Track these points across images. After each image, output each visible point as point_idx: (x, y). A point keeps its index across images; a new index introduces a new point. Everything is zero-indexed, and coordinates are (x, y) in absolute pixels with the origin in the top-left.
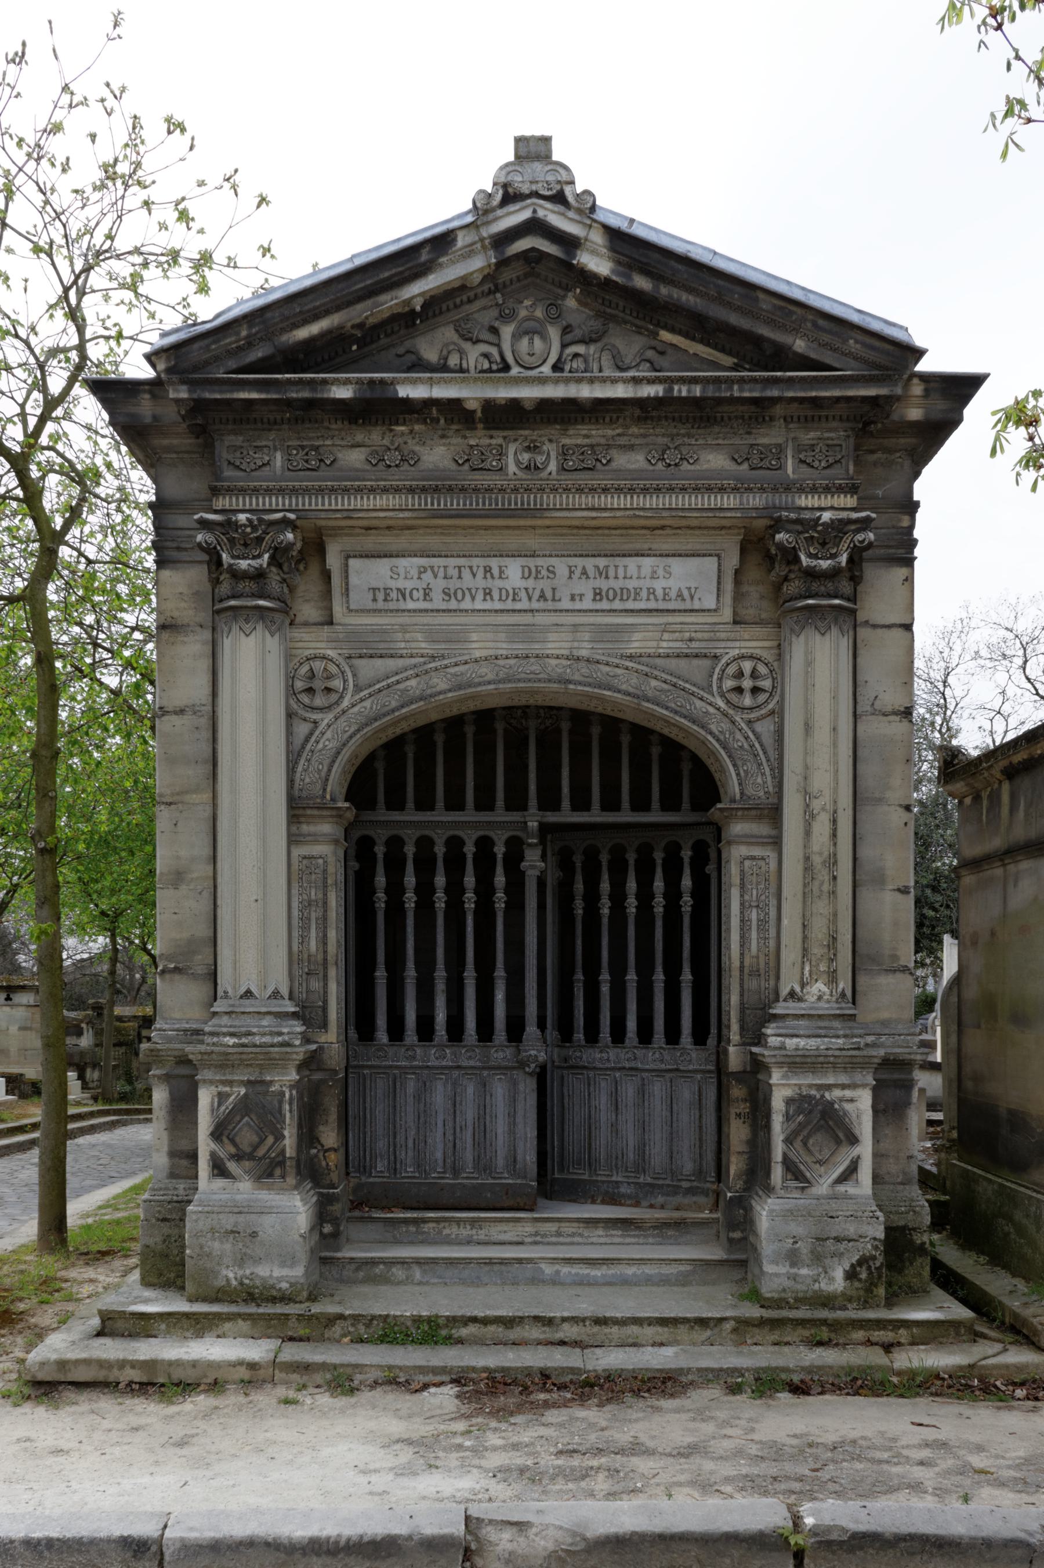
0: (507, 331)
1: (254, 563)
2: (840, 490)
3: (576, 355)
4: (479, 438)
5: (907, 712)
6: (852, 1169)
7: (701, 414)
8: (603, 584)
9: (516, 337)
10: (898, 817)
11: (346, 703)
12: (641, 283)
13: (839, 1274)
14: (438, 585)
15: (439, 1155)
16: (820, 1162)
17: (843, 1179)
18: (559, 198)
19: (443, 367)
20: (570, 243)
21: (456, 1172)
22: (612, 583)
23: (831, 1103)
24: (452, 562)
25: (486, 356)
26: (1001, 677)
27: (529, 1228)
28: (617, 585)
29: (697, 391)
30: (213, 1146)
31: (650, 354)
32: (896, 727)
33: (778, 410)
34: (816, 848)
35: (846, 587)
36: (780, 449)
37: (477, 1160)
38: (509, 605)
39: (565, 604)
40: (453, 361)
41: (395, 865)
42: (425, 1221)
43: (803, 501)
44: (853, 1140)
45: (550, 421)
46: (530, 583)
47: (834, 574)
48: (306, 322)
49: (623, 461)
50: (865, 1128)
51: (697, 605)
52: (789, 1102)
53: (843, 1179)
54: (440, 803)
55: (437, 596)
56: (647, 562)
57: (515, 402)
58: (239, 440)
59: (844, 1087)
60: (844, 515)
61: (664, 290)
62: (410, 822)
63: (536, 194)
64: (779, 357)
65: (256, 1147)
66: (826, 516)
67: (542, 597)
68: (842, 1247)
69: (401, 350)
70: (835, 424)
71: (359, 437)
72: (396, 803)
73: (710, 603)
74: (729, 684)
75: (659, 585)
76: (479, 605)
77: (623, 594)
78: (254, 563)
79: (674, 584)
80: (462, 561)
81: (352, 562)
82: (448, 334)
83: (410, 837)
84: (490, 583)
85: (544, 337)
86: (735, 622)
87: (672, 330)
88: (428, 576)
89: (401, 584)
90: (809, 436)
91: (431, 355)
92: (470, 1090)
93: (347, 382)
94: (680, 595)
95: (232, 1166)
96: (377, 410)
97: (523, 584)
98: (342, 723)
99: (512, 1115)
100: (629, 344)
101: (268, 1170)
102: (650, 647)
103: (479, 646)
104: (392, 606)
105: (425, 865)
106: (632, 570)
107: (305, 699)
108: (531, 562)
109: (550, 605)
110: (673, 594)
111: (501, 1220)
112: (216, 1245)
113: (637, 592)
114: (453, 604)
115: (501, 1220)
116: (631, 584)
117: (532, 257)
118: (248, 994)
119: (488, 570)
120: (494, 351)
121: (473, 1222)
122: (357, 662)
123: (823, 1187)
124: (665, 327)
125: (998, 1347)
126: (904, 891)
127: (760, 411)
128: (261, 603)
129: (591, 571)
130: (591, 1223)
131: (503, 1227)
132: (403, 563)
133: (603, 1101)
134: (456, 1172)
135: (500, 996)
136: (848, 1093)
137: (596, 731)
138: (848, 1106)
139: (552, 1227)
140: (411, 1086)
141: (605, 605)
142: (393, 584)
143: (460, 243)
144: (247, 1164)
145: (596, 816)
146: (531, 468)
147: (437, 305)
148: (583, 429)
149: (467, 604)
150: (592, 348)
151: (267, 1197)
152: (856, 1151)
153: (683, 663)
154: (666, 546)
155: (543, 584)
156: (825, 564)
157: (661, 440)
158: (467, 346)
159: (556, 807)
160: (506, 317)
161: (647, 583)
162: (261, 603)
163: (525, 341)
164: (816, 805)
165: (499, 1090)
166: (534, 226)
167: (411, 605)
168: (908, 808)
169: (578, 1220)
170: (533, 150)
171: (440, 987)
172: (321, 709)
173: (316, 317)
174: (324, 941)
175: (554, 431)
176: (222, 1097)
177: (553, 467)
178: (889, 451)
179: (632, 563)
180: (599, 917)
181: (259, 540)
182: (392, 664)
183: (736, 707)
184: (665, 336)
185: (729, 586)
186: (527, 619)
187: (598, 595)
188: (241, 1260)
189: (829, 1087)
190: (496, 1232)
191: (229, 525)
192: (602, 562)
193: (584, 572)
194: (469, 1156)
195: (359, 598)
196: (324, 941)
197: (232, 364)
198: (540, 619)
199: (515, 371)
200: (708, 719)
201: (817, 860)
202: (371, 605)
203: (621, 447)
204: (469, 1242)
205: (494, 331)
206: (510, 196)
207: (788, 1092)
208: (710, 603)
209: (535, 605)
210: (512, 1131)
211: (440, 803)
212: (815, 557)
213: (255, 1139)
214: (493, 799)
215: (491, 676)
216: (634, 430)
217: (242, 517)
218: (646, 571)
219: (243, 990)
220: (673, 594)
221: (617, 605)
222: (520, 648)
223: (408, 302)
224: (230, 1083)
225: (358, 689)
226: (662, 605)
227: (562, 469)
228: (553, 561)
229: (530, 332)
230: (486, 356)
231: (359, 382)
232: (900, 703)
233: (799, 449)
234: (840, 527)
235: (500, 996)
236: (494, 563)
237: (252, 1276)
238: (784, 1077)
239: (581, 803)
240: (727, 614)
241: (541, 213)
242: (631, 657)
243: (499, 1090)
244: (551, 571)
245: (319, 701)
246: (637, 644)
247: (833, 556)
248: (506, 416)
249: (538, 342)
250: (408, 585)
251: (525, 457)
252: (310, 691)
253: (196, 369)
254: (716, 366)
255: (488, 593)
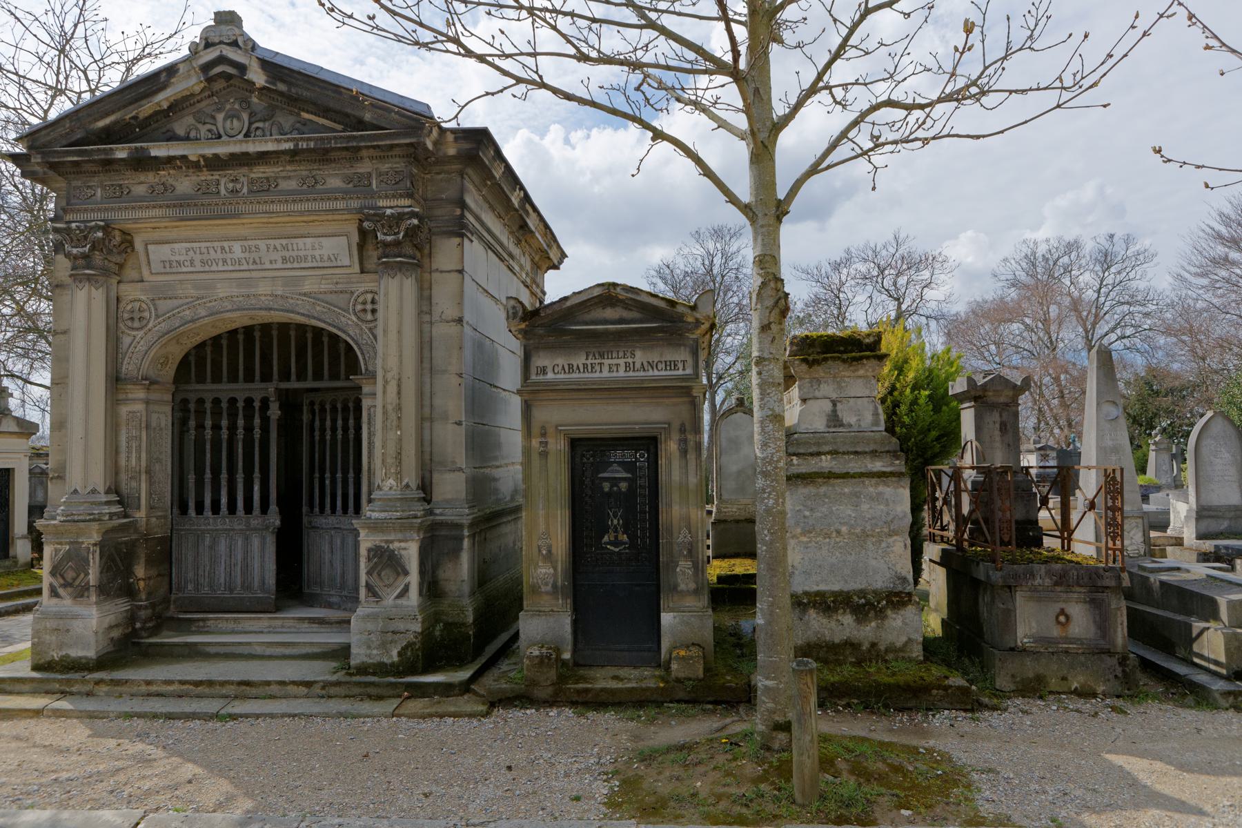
0: (220, 117)
1: (81, 250)
2: (401, 196)
3: (257, 128)
4: (205, 176)
5: (460, 321)
6: (406, 589)
7: (323, 155)
8: (287, 254)
9: (225, 119)
10: (455, 380)
11: (150, 325)
12: (282, 87)
13: (395, 653)
14: (198, 258)
15: (222, 580)
16: (388, 586)
17: (400, 596)
18: (235, 44)
19: (187, 138)
20: (242, 68)
21: (231, 591)
22: (291, 253)
23: (393, 551)
24: (203, 245)
25: (209, 131)
26: (869, 288)
27: (266, 623)
28: (294, 254)
29: (312, 145)
30: (51, 579)
31: (298, 125)
32: (453, 329)
33: (364, 153)
34: (389, 400)
35: (408, 250)
36: (370, 174)
37: (243, 583)
38: (237, 267)
39: (268, 266)
40: (193, 134)
41: (200, 413)
42: (208, 619)
43: (381, 203)
44: (406, 573)
45: (242, 165)
46: (247, 255)
47: (397, 243)
48: (102, 118)
49: (284, 185)
50: (413, 566)
51: (339, 264)
52: (369, 550)
53: (400, 596)
54: (209, 380)
55: (197, 263)
56: (309, 241)
57: (216, 156)
58: (79, 183)
59: (400, 541)
60: (400, 210)
61: (293, 90)
62: (209, 390)
63: (221, 43)
64: (361, 124)
65: (74, 580)
66: (389, 212)
67: (254, 262)
68: (396, 637)
69: (164, 130)
70: (398, 159)
71: (142, 178)
72: (201, 379)
73: (346, 262)
74: (359, 307)
75: (317, 253)
76: (221, 268)
77: (299, 259)
78: (81, 250)
79: (326, 252)
80: (208, 244)
81: (149, 247)
82: (190, 120)
83: (209, 398)
84: (225, 256)
85: (239, 119)
86: (362, 272)
87: (307, 112)
88: (191, 253)
89: (177, 258)
90: (385, 167)
91: (181, 131)
92: (240, 543)
93: (123, 149)
94: (329, 258)
95: (61, 591)
96: (141, 163)
97: (243, 255)
98: (149, 336)
99: (262, 557)
100: (287, 121)
101: (80, 593)
102: (315, 288)
103: (222, 291)
104: (174, 270)
105: (217, 413)
106: (301, 246)
107: (129, 323)
108: (245, 243)
109: (259, 267)
110: (325, 258)
111: (250, 619)
112: (48, 637)
113: (306, 257)
114: (207, 268)
115: (250, 619)
116: (302, 253)
117: (223, 75)
118: (76, 491)
119: (223, 248)
120: (214, 128)
121: (235, 619)
122: (157, 302)
123: (389, 600)
124: (303, 110)
125: (396, 702)
126: (459, 423)
127: (353, 153)
128: (87, 272)
129: (279, 247)
130: (312, 620)
131: (252, 623)
132: (176, 246)
133: (326, 548)
134: (231, 591)
135: (256, 488)
136: (403, 545)
137: (309, 336)
138: (403, 552)
139: (279, 623)
140: (208, 541)
141: (289, 265)
142: (173, 258)
143: (181, 71)
144: (70, 589)
145: (310, 384)
146: (234, 192)
147: (176, 107)
148: (262, 169)
149: (214, 268)
150: (267, 124)
151: (78, 609)
152: (408, 579)
153: (334, 296)
154: (320, 230)
155: (254, 255)
156: (389, 238)
157: (304, 173)
158: (200, 126)
159: (288, 379)
160: (219, 110)
161: (310, 253)
162: (87, 272)
163: (229, 122)
164: (389, 376)
165: (256, 542)
166: (222, 60)
167: (184, 269)
168: (460, 375)
169: (293, 618)
170: (228, 19)
171: (224, 483)
172: (137, 329)
173: (107, 115)
174: (139, 459)
175: (244, 170)
176: (57, 551)
177: (245, 190)
178: (449, 173)
179: (300, 241)
180: (253, 441)
181: (86, 237)
182: (176, 302)
183: (363, 321)
184: (305, 115)
185: (355, 253)
186: (247, 275)
187: (284, 260)
188: (61, 646)
189: (392, 542)
190: (248, 625)
191: (68, 231)
192: (284, 242)
193: (275, 248)
194: (239, 581)
195: (156, 267)
196: (139, 459)
197: (64, 142)
198: (254, 274)
199: (224, 138)
200: (348, 327)
201: (390, 408)
202: (163, 270)
203: (284, 178)
204: (233, 632)
205: (214, 118)
206: (208, 44)
207: (369, 545)
208: (346, 262)
209: (251, 267)
210: (262, 567)
211: (209, 380)
212: (385, 234)
213: (75, 575)
214: (254, 376)
215: (230, 307)
216: (288, 168)
217: (74, 225)
218: (309, 246)
219: (89, 489)
220: (325, 258)
221: (296, 265)
222: (244, 291)
223: (158, 104)
224: (61, 544)
225: (157, 316)
226: (320, 265)
227: (250, 191)
228: (258, 242)
229: (232, 117)
230: (209, 131)
231: (130, 148)
232: (456, 315)
233: (380, 174)
234: (400, 217)
235: (256, 488)
236: (226, 244)
237: (67, 656)
238: (367, 535)
239: (301, 376)
240: (357, 268)
241: (224, 53)
242: (305, 295)
243: (256, 542)
244: (257, 247)
245: (136, 324)
246: (307, 288)
247: (395, 234)
248: (215, 163)
249: (235, 121)
250: (182, 258)
251: (231, 185)
252: (132, 319)
253: (45, 146)
254: (334, 130)
255: (225, 261)
